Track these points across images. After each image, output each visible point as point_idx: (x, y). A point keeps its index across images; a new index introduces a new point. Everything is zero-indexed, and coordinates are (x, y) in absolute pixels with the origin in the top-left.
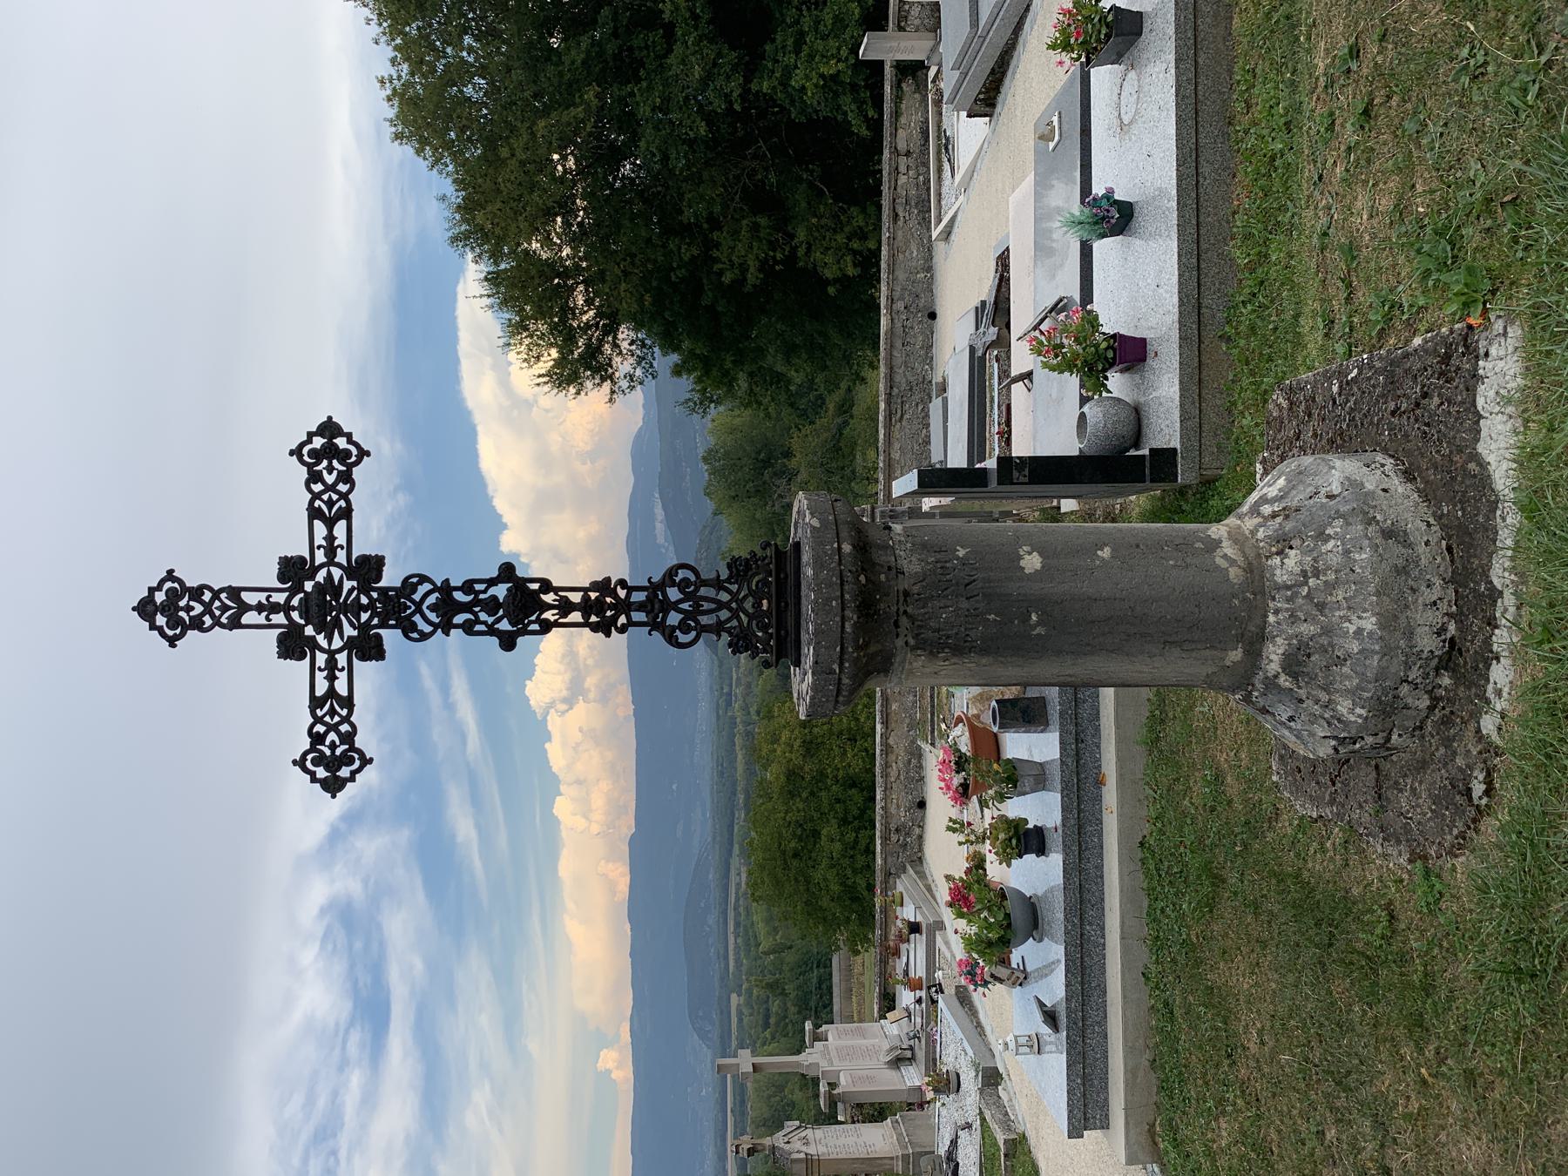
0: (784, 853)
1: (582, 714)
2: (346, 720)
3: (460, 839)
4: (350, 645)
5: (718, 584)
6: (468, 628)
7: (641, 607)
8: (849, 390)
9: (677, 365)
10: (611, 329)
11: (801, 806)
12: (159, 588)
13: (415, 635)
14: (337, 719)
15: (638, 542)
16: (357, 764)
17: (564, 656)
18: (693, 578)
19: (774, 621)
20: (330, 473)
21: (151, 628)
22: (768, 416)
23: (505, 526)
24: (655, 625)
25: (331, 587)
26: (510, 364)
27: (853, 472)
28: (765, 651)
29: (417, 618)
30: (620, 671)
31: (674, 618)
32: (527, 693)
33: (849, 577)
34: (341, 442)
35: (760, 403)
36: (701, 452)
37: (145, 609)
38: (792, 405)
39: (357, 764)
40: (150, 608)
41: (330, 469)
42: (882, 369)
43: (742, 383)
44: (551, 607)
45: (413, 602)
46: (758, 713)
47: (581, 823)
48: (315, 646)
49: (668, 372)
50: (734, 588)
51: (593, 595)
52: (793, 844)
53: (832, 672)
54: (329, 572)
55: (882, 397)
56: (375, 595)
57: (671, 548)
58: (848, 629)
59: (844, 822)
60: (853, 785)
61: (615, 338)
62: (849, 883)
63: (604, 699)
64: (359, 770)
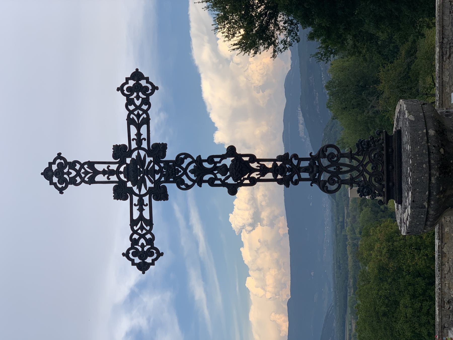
0: (377, 313)
1: (260, 232)
2: (149, 232)
3: (197, 298)
4: (150, 192)
5: (351, 156)
6: (211, 183)
7: (306, 170)
8: (414, 42)
9: (311, 34)
10: (274, 16)
11: (387, 287)
12: (54, 163)
13: (183, 187)
14: (144, 231)
15: (288, 135)
16: (155, 256)
17: (249, 200)
18: (336, 153)
19: (385, 177)
20: (138, 100)
21: (51, 184)
22: (365, 60)
23: (216, 129)
24: (314, 180)
25: (140, 161)
26: (218, 39)
27: (417, 91)
28: (380, 195)
29: (184, 177)
30: (280, 209)
31: (325, 176)
32: (230, 220)
33: (433, 149)
34: (143, 83)
35: (360, 53)
36: (324, 83)
37: (47, 174)
38: (379, 52)
39: (155, 256)
40: (50, 173)
41: (138, 97)
42: (437, 28)
43: (350, 41)
44: (255, 170)
45: (182, 168)
46: (360, 233)
47: (261, 292)
48: (132, 193)
49: (306, 38)
50: (361, 158)
51: (279, 163)
52: (383, 308)
53: (424, 207)
54: (138, 153)
55: (437, 44)
56: (162, 165)
57: (308, 139)
58: (433, 180)
59: (414, 296)
60: (419, 275)
61: (276, 20)
62: (417, 331)
63: (272, 224)
64: (156, 259)
